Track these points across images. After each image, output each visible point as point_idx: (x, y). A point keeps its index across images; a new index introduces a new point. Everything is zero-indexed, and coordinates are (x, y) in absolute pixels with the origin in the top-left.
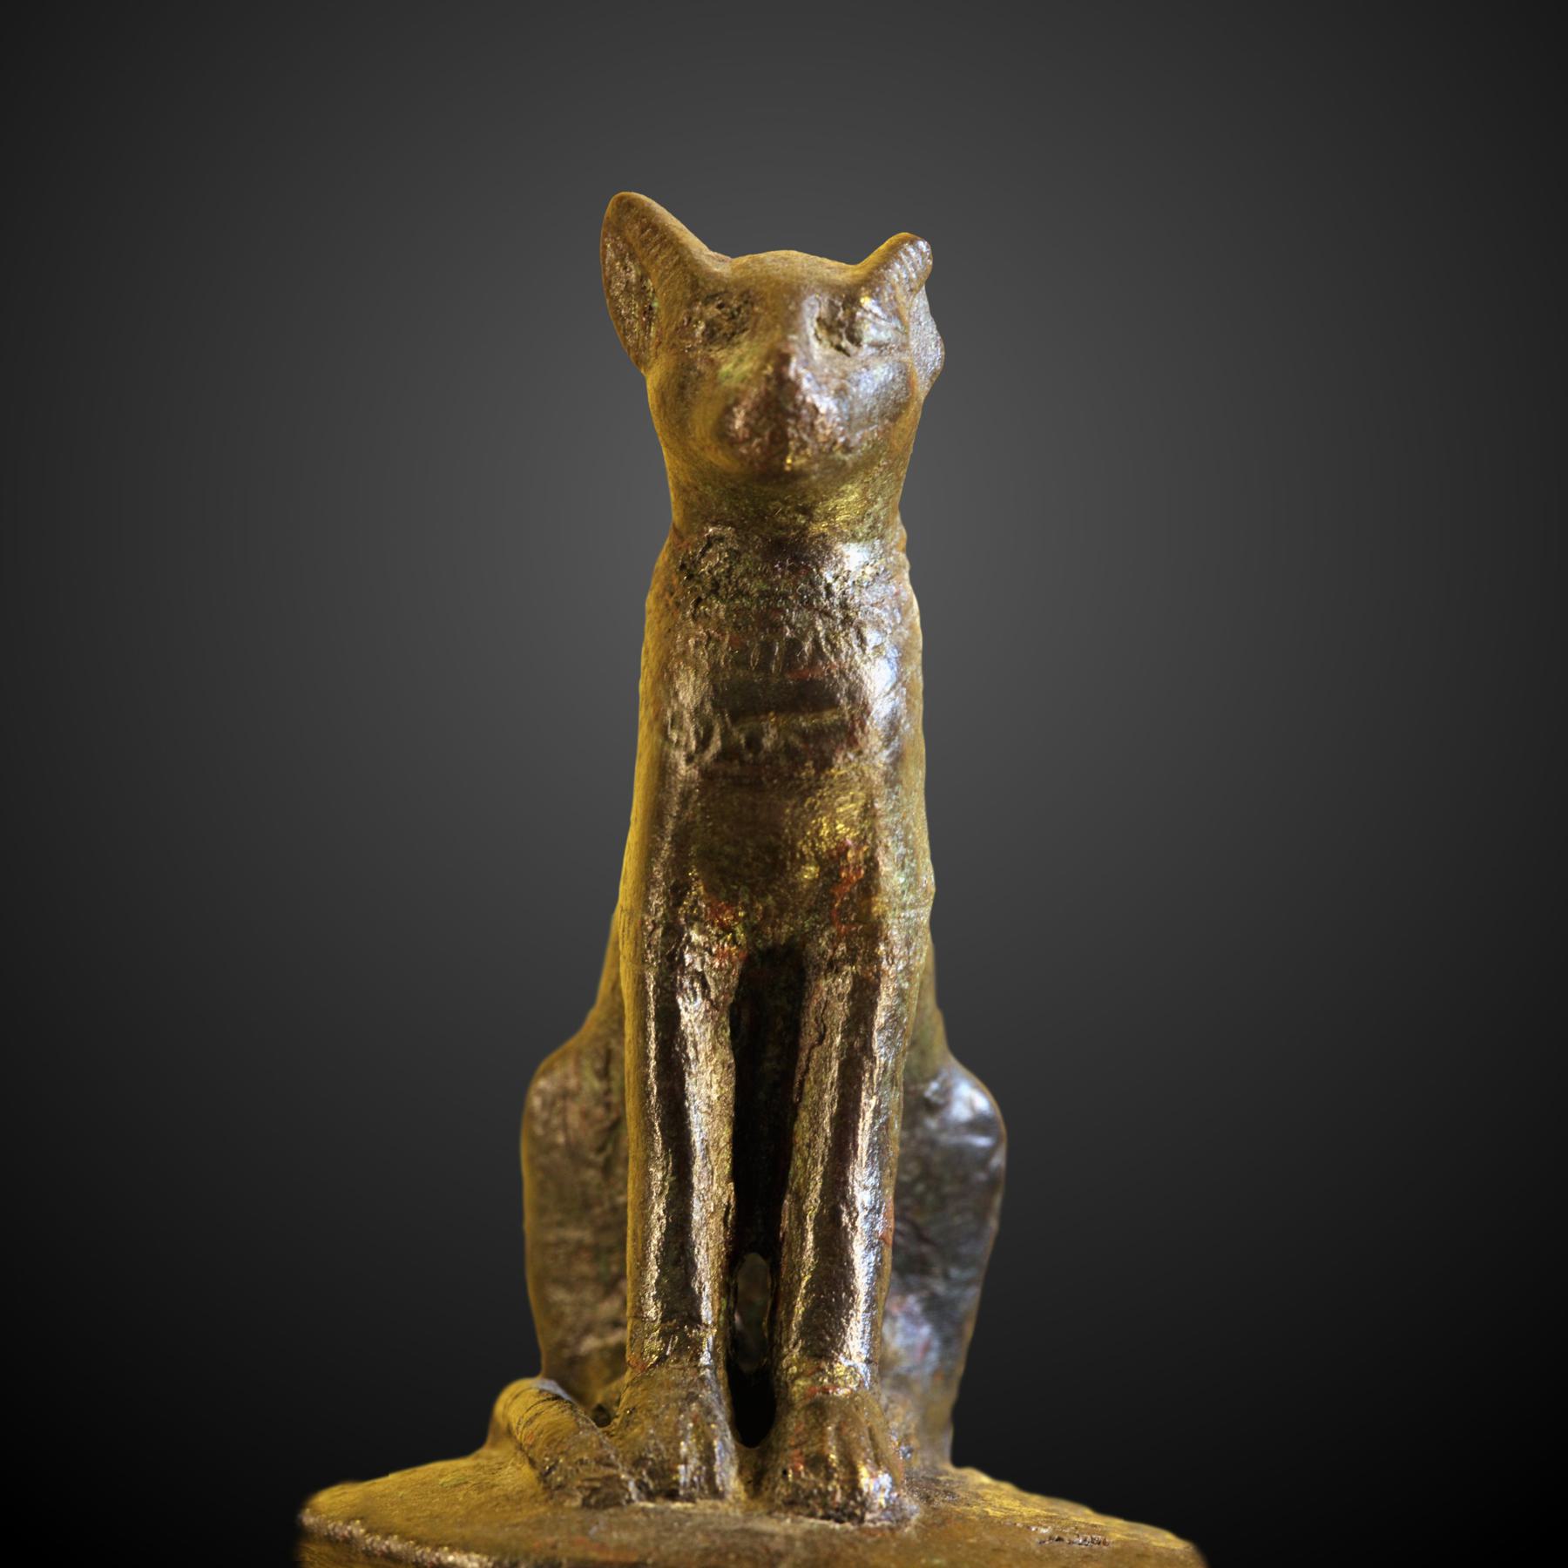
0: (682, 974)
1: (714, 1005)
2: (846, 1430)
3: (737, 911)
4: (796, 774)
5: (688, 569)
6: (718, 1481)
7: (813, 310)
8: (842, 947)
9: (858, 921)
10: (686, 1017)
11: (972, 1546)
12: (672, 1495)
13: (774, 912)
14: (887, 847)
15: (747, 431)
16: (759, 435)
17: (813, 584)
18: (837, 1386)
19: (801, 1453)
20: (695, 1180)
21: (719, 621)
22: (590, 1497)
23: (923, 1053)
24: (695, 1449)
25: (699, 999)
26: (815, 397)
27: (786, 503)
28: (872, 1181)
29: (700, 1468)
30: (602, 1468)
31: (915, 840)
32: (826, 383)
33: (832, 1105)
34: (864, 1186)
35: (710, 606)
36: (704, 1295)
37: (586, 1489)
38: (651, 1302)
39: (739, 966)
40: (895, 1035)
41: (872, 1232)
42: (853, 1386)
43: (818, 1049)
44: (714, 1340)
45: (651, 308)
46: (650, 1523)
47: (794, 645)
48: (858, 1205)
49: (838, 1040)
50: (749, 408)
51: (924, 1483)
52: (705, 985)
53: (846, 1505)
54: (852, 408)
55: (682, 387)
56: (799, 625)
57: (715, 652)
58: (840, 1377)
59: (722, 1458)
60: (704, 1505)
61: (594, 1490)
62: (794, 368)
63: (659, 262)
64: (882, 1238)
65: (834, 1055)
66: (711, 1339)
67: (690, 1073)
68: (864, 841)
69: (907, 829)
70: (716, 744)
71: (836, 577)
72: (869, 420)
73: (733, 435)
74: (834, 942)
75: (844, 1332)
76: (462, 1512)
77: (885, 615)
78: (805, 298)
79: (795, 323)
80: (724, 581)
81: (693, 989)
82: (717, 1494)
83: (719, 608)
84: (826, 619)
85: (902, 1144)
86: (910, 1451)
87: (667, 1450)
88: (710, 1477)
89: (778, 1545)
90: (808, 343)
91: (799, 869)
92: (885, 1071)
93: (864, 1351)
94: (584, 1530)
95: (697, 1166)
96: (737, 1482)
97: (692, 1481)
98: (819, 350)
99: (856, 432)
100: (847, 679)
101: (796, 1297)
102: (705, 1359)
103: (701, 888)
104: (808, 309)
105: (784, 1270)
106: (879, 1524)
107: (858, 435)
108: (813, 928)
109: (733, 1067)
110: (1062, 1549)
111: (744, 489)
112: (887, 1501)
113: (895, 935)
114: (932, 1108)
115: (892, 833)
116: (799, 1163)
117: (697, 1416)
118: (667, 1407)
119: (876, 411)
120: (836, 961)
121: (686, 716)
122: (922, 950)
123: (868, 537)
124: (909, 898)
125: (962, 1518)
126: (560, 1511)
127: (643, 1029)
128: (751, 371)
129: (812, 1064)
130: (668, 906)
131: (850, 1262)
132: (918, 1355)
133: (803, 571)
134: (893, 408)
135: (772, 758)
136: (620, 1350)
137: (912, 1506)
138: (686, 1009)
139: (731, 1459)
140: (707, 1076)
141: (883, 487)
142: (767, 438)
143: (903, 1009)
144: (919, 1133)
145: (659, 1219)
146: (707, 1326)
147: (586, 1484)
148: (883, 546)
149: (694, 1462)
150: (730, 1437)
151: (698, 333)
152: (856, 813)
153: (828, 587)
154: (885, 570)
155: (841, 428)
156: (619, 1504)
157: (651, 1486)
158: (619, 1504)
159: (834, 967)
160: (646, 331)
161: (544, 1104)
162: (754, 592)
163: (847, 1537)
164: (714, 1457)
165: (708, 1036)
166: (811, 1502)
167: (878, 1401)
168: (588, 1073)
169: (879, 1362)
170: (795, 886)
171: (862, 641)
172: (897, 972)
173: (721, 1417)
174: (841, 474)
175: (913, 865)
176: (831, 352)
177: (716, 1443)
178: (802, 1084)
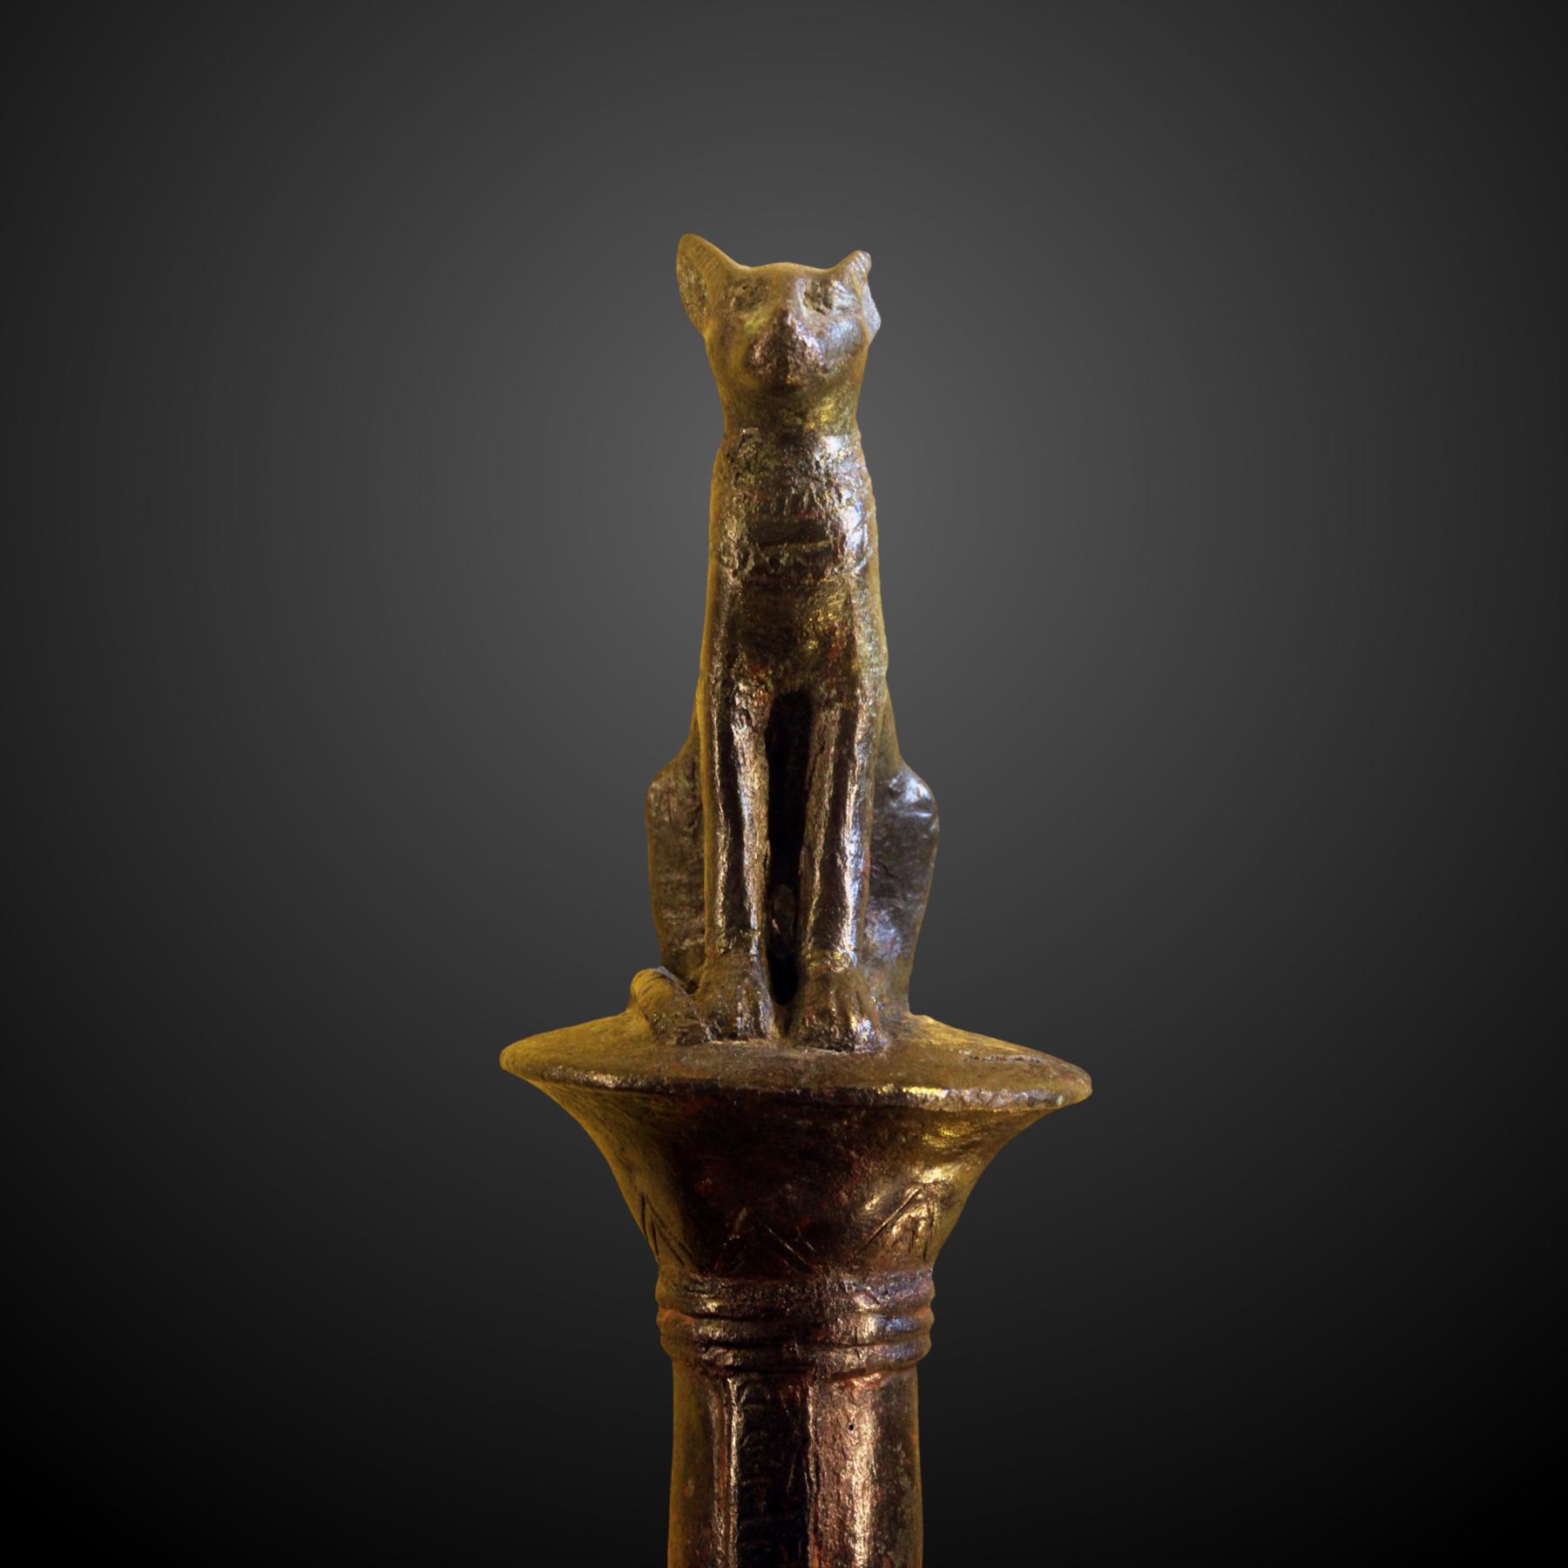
0: (734, 711)
1: (755, 730)
2: (842, 993)
3: (767, 671)
4: (802, 582)
5: (732, 457)
6: (762, 1027)
7: (801, 289)
8: (834, 692)
9: (843, 675)
10: (737, 738)
11: (922, 1064)
12: (733, 1036)
13: (791, 670)
14: (860, 628)
15: (762, 359)
16: (770, 362)
17: (808, 462)
18: (836, 966)
19: (814, 1008)
20: (745, 840)
21: (751, 486)
22: (681, 1038)
23: (887, 761)
24: (747, 1007)
25: (745, 726)
26: (805, 337)
27: (789, 410)
28: (855, 838)
29: (750, 1019)
30: (689, 1020)
31: (877, 625)
32: (811, 329)
33: (829, 791)
34: (851, 841)
35: (745, 478)
36: (752, 911)
37: (680, 1033)
38: (719, 916)
39: (769, 705)
40: (868, 746)
41: (856, 869)
42: (846, 966)
43: (820, 755)
44: (759, 939)
45: (704, 297)
46: (719, 1054)
47: (798, 498)
48: (847, 853)
49: (833, 749)
50: (764, 345)
51: (892, 1025)
52: (748, 717)
53: (843, 1040)
54: (827, 345)
55: (723, 338)
56: (799, 486)
57: (749, 504)
58: (838, 960)
59: (764, 1014)
60: (754, 1042)
61: (684, 1034)
62: (790, 320)
63: (707, 267)
64: (863, 873)
65: (830, 759)
66: (757, 938)
67: (740, 773)
68: (846, 624)
69: (873, 617)
70: (751, 563)
71: (822, 457)
72: (838, 353)
73: (754, 362)
74: (828, 689)
75: (840, 932)
76: (603, 1049)
77: (852, 480)
78: (796, 280)
79: (790, 293)
80: (754, 461)
81: (741, 720)
82: (761, 1035)
83: (750, 478)
84: (816, 482)
85: (875, 817)
86: (884, 1005)
87: (730, 1007)
88: (757, 1024)
89: (800, 1066)
90: (799, 306)
91: (805, 643)
92: (862, 769)
93: (852, 943)
94: (678, 1060)
95: (746, 831)
96: (774, 1027)
97: (746, 1027)
98: (806, 312)
99: (831, 359)
100: (831, 519)
101: (809, 911)
102: (753, 951)
103: (744, 656)
104: (798, 287)
105: (802, 894)
106: (863, 1052)
107: (832, 362)
108: (816, 681)
109: (767, 769)
110: (978, 1064)
111: (763, 401)
112: (868, 1037)
113: (867, 683)
114: (894, 794)
115: (863, 619)
116: (810, 827)
117: (748, 986)
118: (730, 981)
119: (843, 348)
120: (830, 700)
121: (732, 545)
122: (884, 693)
123: (841, 433)
124: (874, 660)
125: (916, 1046)
126: (663, 1047)
127: (710, 747)
128: (764, 323)
129: (817, 766)
130: (724, 669)
131: (843, 888)
132: (889, 946)
133: (802, 453)
134: (853, 348)
135: (787, 569)
136: (702, 947)
137: (884, 1039)
138: (737, 732)
139: (771, 1013)
140: (751, 774)
141: (848, 401)
142: (775, 363)
143: (872, 730)
144: (886, 810)
145: (723, 864)
146: (754, 930)
147: (679, 1030)
148: (851, 439)
149: (746, 1016)
150: (769, 999)
151: (732, 305)
152: (840, 606)
153: (817, 463)
154: (852, 454)
155: (821, 357)
156: (699, 1042)
157: (720, 1031)
158: (699, 1042)
159: (829, 704)
160: (701, 311)
161: (655, 797)
162: (772, 467)
163: (844, 1060)
164: (759, 1012)
165: (751, 749)
166: (820, 1039)
167: (862, 974)
168: (681, 777)
169: (863, 951)
170: (803, 654)
171: (840, 496)
172: (869, 707)
173: (764, 987)
174: (822, 388)
175: (877, 639)
176: (815, 312)
177: (760, 1003)
178: (811, 778)
